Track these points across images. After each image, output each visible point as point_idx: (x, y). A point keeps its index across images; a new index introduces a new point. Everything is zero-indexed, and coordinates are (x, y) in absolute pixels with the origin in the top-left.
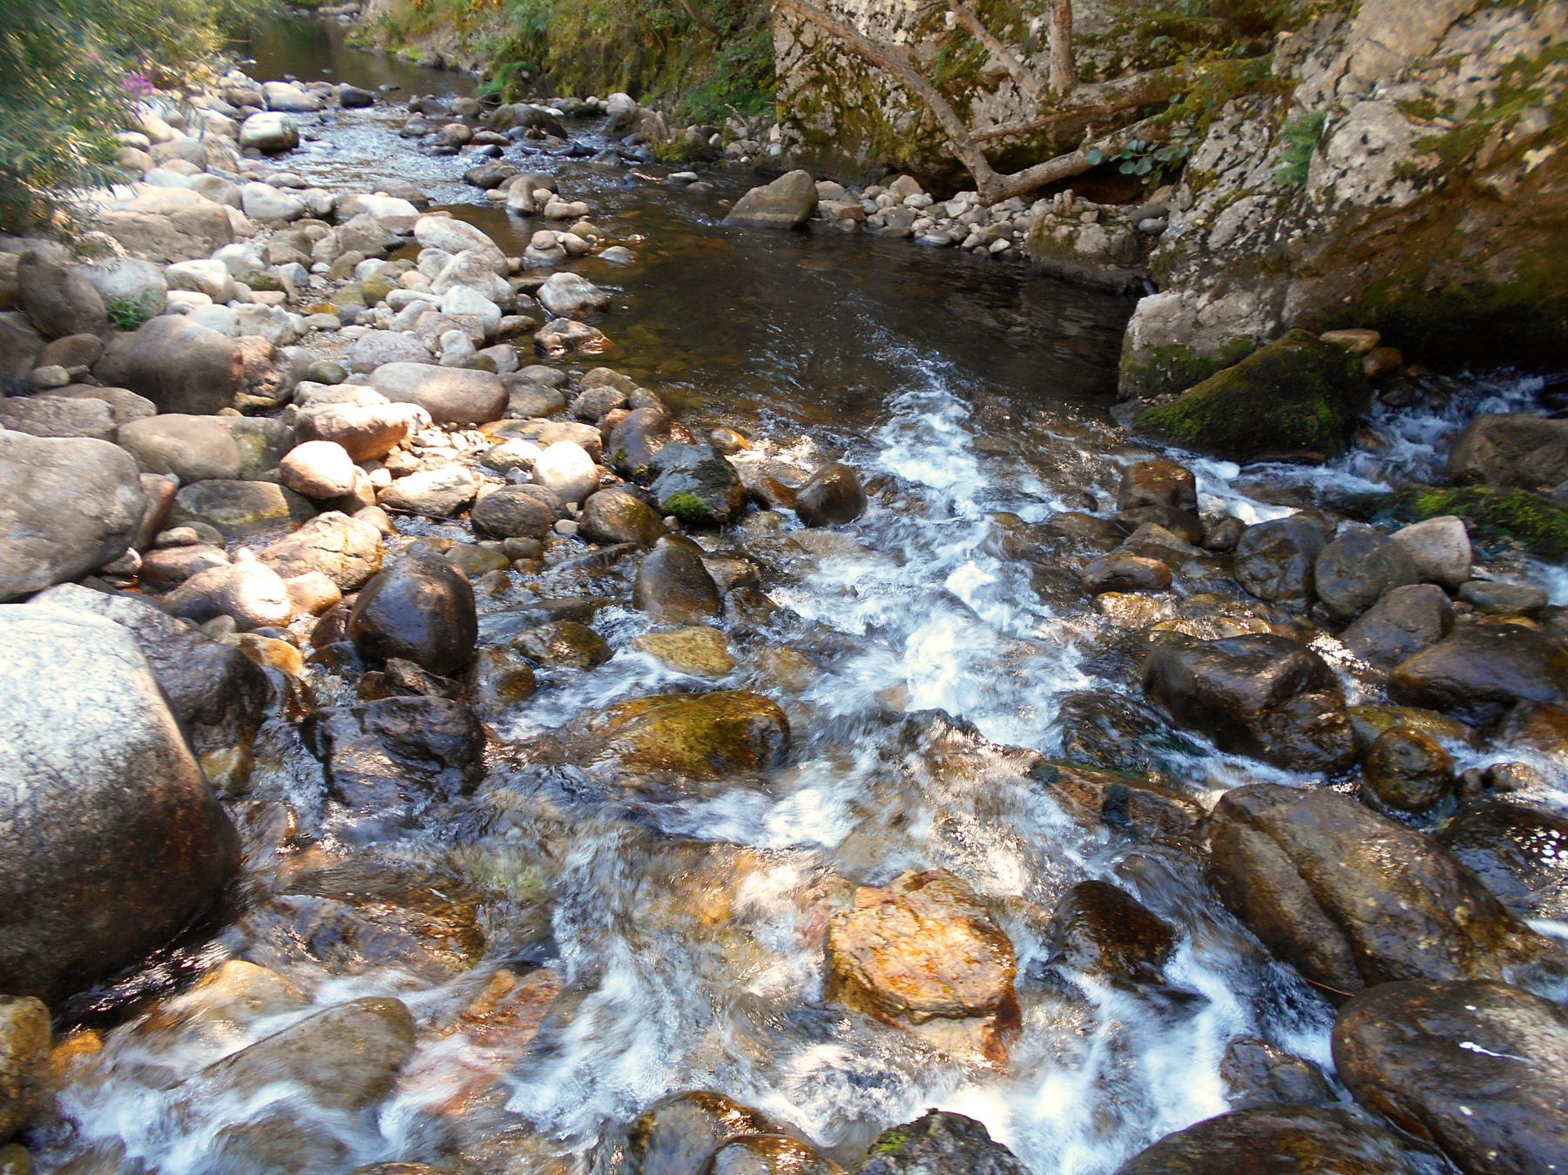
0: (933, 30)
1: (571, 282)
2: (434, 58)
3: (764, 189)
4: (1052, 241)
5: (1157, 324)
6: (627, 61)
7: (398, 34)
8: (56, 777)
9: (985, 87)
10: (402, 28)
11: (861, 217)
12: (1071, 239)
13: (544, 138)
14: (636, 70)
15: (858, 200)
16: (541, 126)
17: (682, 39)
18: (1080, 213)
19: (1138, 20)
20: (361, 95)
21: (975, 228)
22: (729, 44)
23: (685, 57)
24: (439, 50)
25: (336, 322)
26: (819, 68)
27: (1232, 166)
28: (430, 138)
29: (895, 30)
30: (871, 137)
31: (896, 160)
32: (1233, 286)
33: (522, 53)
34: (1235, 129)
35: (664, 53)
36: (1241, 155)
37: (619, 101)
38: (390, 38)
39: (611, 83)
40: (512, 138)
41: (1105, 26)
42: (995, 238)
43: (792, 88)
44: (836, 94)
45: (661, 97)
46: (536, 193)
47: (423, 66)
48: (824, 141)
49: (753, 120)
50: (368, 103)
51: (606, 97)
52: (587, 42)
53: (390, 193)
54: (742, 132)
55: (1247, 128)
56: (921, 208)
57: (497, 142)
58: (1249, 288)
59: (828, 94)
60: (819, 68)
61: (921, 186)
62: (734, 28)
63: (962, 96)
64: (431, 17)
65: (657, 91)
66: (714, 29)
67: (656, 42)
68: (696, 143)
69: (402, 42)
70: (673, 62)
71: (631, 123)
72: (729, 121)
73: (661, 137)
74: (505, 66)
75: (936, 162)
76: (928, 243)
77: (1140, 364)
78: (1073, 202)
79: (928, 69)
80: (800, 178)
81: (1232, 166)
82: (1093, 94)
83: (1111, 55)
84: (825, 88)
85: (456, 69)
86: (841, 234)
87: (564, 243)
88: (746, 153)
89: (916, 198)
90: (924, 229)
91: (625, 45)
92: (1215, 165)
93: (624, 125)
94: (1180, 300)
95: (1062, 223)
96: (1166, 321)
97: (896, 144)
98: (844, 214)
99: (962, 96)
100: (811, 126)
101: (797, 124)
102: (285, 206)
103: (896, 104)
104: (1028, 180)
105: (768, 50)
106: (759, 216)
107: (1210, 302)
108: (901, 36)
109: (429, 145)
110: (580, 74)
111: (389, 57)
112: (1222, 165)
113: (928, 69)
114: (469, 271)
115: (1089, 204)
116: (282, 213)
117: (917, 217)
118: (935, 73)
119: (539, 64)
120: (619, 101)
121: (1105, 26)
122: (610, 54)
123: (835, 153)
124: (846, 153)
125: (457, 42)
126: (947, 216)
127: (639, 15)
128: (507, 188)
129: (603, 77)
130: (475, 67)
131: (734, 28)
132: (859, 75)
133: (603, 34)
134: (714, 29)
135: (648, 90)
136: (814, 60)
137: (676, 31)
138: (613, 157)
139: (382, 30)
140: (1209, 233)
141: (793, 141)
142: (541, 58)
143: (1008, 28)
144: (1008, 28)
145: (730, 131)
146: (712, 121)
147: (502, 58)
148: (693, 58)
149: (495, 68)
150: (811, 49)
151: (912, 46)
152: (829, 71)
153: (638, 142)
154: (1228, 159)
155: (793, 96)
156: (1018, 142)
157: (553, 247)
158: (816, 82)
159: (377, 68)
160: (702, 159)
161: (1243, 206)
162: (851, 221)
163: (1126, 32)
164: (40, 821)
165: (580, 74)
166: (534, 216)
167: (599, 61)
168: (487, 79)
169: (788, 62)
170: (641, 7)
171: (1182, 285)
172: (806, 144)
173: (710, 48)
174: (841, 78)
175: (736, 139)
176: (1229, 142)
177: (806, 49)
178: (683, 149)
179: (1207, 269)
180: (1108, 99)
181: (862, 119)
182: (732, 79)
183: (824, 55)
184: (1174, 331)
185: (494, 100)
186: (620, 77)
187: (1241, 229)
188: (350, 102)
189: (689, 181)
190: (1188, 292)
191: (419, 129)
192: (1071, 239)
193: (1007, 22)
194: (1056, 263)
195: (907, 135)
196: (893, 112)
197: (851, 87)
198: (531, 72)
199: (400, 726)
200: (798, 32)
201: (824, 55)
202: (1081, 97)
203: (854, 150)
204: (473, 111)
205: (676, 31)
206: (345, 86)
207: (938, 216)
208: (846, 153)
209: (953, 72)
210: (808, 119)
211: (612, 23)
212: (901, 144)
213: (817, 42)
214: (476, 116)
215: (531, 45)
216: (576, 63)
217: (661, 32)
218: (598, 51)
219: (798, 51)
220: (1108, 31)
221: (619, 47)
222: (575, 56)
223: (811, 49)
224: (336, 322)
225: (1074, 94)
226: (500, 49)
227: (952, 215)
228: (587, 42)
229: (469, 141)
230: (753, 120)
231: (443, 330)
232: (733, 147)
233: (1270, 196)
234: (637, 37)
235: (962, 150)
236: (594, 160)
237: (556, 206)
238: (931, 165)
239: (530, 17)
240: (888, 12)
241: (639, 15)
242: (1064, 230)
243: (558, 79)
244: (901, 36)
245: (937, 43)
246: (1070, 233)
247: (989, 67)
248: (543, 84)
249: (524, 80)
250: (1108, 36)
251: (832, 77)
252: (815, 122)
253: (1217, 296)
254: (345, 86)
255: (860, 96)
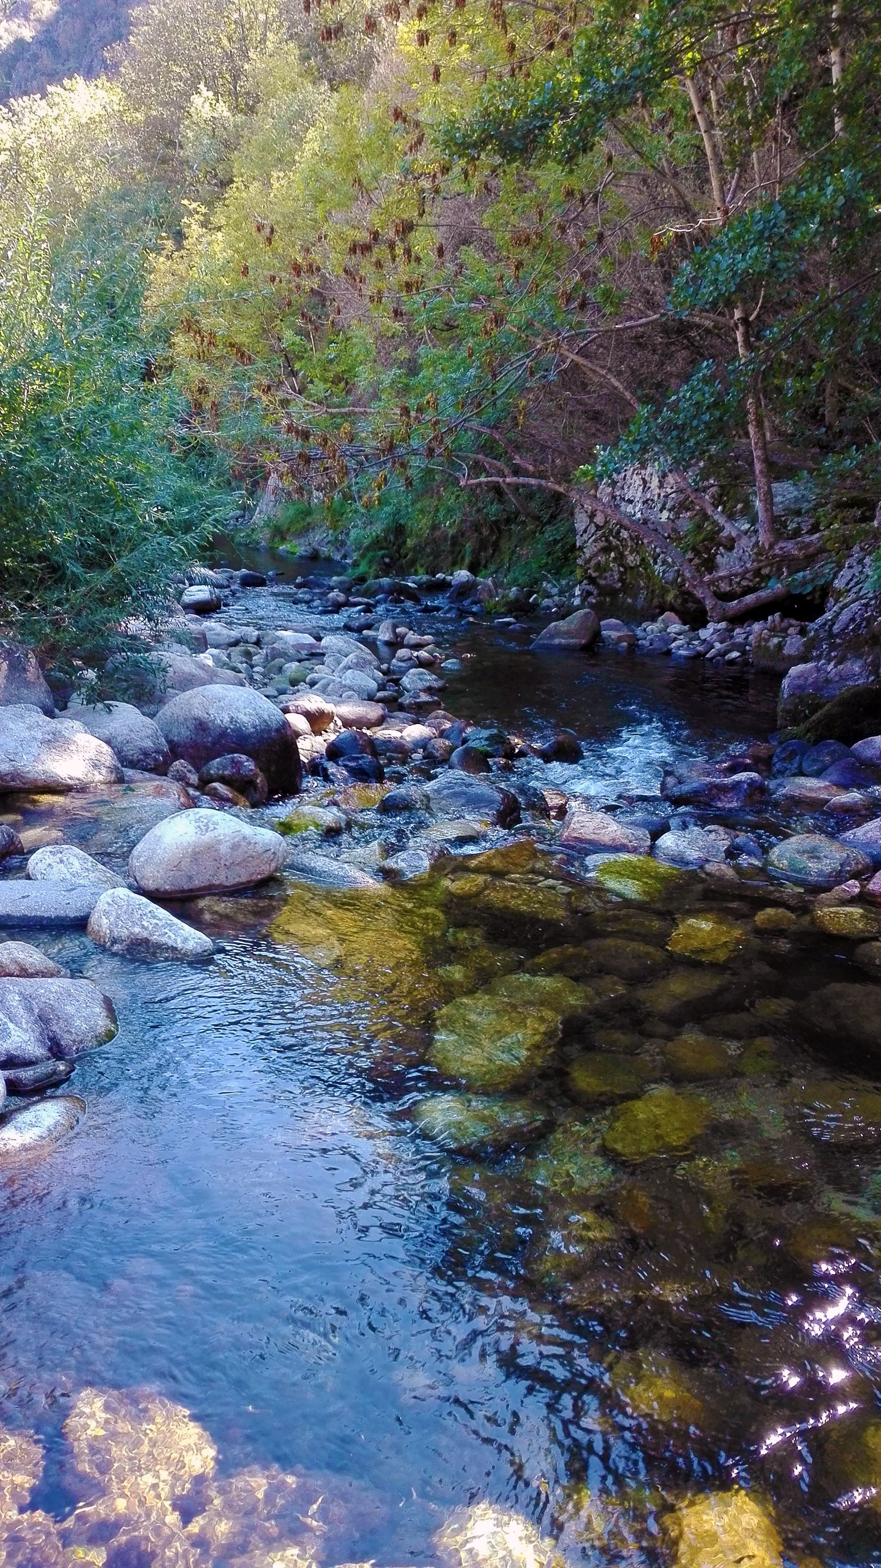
0: (688, 510)
1: (421, 674)
2: (310, 550)
3: (561, 623)
4: (767, 648)
5: (801, 682)
6: (468, 546)
7: (280, 533)
8: (265, 721)
9: (725, 547)
10: (285, 528)
11: (634, 644)
12: (780, 647)
13: (403, 602)
14: (476, 553)
15: (633, 631)
16: (398, 593)
17: (513, 527)
18: (787, 629)
19: (834, 497)
20: (257, 577)
21: (718, 645)
22: (549, 528)
23: (514, 540)
24: (315, 544)
25: (276, 693)
26: (607, 540)
27: (857, 584)
28: (317, 603)
29: (661, 511)
30: (648, 587)
31: (665, 602)
32: (849, 656)
33: (384, 544)
34: (860, 562)
35: (498, 539)
36: (863, 577)
37: (462, 575)
38: (273, 537)
39: (456, 564)
40: (378, 602)
41: (809, 502)
42: (730, 651)
43: (588, 556)
44: (620, 559)
45: (496, 572)
46: (398, 630)
47: (301, 557)
48: (613, 593)
49: (564, 582)
50: (262, 583)
51: (451, 574)
52: (438, 533)
53: (296, 631)
54: (555, 591)
55: (867, 560)
56: (679, 634)
57: (367, 604)
58: (859, 656)
59: (615, 559)
60: (607, 540)
61: (680, 618)
62: (553, 517)
63: (709, 554)
64: (309, 519)
65: (492, 567)
66: (537, 518)
67: (492, 531)
68: (517, 600)
69: (283, 539)
70: (505, 545)
71: (470, 590)
72: (545, 584)
73: (491, 596)
74: (370, 555)
75: (693, 602)
76: (681, 656)
77: (789, 707)
78: (782, 621)
79: (686, 536)
80: (586, 614)
81: (857, 584)
82: (790, 547)
83: (812, 521)
84: (613, 555)
85: (329, 560)
86: (618, 653)
87: (417, 657)
88: (556, 606)
89: (675, 627)
90: (678, 648)
91: (468, 534)
92: (847, 584)
93: (465, 590)
94: (816, 666)
95: (774, 636)
96: (806, 679)
97: (664, 591)
98: (620, 639)
99: (709, 554)
100: (602, 582)
101: (592, 581)
102: (229, 636)
103: (664, 562)
104: (742, 605)
105: (573, 531)
106: (557, 641)
107: (835, 666)
108: (665, 515)
109: (317, 607)
110: (431, 558)
111: (272, 551)
112: (852, 584)
113: (686, 536)
114: (357, 664)
115: (793, 622)
116: (227, 641)
117: (675, 639)
118: (690, 540)
119: (398, 551)
120: (462, 575)
121: (809, 502)
122: (456, 541)
123: (621, 601)
124: (629, 600)
125: (330, 538)
126: (699, 639)
127: (479, 511)
128: (377, 629)
129: (450, 558)
130: (345, 557)
131: (553, 517)
132: (637, 544)
133: (450, 527)
134: (537, 518)
135: (485, 567)
136: (603, 535)
137: (508, 521)
138: (454, 611)
139: (267, 531)
140: (834, 624)
141: (589, 594)
142: (400, 547)
143: (740, 506)
144: (740, 506)
145: (545, 591)
146: (533, 585)
147: (368, 549)
148: (521, 541)
149: (363, 556)
150: (602, 527)
151: (673, 521)
152: (615, 542)
153: (475, 603)
154: (855, 580)
155: (588, 561)
156: (751, 584)
157: (410, 659)
158: (606, 550)
159: (262, 559)
160: (522, 610)
161: (855, 606)
162: (625, 644)
163: (822, 505)
164: (262, 731)
165: (431, 558)
166: (395, 644)
167: (447, 546)
168: (356, 564)
169: (585, 537)
170: (480, 505)
171: (819, 658)
172: (599, 595)
173: (535, 532)
174: (625, 547)
175: (549, 596)
176: (856, 570)
177: (598, 528)
178: (507, 604)
179: (833, 647)
180: (800, 549)
181: (640, 575)
182: (549, 554)
183: (611, 531)
184: (810, 685)
185: (362, 579)
186: (463, 559)
187: (853, 620)
188: (248, 582)
189: (509, 624)
190: (823, 661)
191: (307, 597)
192: (780, 647)
193: (738, 502)
194: (770, 664)
195: (672, 584)
196: (662, 569)
197: (631, 553)
198: (391, 558)
199: (352, 764)
200: (592, 516)
201: (611, 531)
202: (781, 549)
203: (635, 597)
204: (346, 586)
205: (508, 521)
206: (244, 571)
207: (691, 639)
208: (629, 600)
209: (701, 537)
210: (600, 577)
211: (458, 517)
212: (668, 591)
213: (606, 522)
214: (349, 589)
215: (392, 538)
216: (428, 550)
217: (496, 522)
218: (446, 540)
219: (593, 529)
220: (811, 505)
221: (463, 535)
222: (427, 544)
223: (602, 527)
224: (276, 693)
225: (777, 547)
226: (366, 543)
227: (703, 638)
228: (438, 533)
229: (348, 604)
230: (564, 582)
231: (344, 692)
232: (546, 602)
233: (871, 599)
234: (477, 527)
235: (695, 587)
236: (440, 614)
237: (412, 637)
238: (690, 605)
239: (394, 515)
240: (656, 498)
241: (479, 511)
242: (776, 640)
243: (413, 562)
244: (665, 515)
245: (691, 518)
246: (780, 642)
247: (724, 534)
248: (401, 567)
249: (385, 564)
250: (811, 509)
251: (617, 547)
252: (606, 579)
253: (839, 663)
254: (244, 571)
255: (638, 558)
